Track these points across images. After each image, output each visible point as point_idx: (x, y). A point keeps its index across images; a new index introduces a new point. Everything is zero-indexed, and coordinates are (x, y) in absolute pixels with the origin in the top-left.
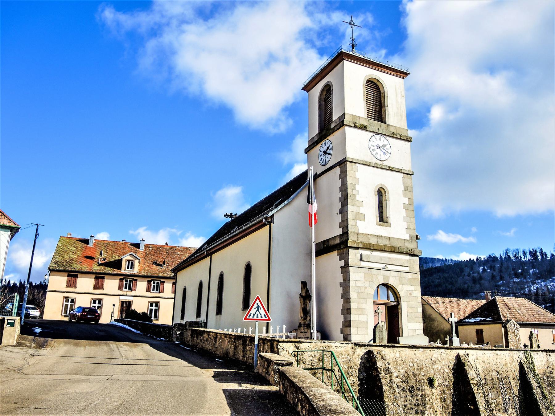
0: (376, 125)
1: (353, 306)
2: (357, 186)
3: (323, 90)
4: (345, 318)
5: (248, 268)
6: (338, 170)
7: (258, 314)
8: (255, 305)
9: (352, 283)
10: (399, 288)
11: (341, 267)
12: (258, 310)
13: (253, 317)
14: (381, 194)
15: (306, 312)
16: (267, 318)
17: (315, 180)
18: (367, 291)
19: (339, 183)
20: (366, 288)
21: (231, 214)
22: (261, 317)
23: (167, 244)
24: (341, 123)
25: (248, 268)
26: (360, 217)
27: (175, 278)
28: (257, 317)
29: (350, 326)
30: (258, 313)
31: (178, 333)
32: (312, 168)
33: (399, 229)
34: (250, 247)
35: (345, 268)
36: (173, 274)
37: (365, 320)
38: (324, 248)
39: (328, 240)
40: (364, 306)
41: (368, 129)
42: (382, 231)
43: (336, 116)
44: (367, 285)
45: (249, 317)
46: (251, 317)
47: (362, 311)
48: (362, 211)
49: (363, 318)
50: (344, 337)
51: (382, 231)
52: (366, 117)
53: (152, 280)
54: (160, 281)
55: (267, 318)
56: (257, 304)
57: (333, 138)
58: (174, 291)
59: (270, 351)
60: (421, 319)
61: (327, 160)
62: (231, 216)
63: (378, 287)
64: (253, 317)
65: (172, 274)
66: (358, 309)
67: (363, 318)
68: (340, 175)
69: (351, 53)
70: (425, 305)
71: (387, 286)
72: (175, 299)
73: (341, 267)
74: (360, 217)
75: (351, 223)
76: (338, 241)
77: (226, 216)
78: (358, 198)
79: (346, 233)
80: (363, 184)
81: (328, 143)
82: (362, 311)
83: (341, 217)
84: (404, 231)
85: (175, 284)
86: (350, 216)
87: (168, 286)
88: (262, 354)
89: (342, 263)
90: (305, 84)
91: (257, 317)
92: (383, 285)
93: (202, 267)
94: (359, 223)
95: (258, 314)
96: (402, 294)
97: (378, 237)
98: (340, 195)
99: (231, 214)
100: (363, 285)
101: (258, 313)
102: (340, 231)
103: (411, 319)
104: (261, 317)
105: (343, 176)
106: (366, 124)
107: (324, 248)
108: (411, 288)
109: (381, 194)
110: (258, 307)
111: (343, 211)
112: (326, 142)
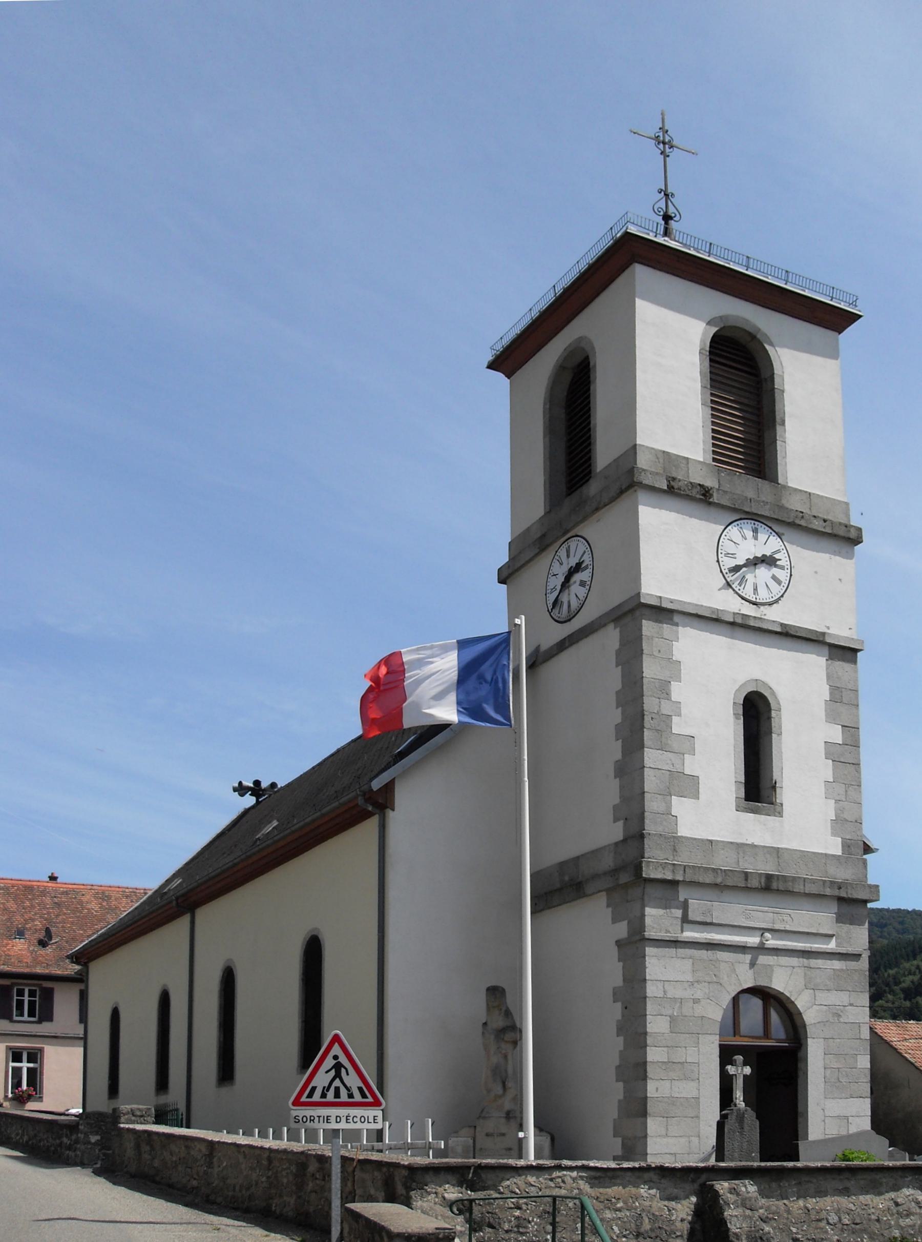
0: (747, 488)
1: (654, 1054)
2: (674, 686)
3: (561, 368)
4: (626, 1091)
5: (313, 952)
6: (611, 637)
7: (337, 1090)
8: (329, 1062)
9: (652, 990)
10: (802, 1002)
11: (619, 943)
12: (338, 1075)
13: (324, 1095)
14: (756, 712)
15: (506, 1078)
16: (370, 1099)
17: (531, 666)
18: (699, 1010)
19: (614, 679)
20: (696, 1001)
21: (257, 783)
22: (351, 1096)
23: (53, 878)
24: (627, 482)
25: (313, 952)
26: (689, 786)
27: (80, 979)
28: (337, 1094)
29: (644, 1114)
30: (337, 1083)
31: (94, 1139)
32: (521, 621)
33: (803, 825)
34: (321, 887)
35: (634, 946)
36: (77, 967)
37: (695, 1094)
38: (559, 888)
39: (576, 860)
40: (691, 1055)
41: (715, 498)
42: (755, 829)
43: (604, 455)
44: (699, 994)
45: (310, 1095)
46: (317, 1097)
47: (682, 1070)
48: (691, 766)
49: (685, 1090)
50: (623, 1144)
51: (755, 829)
52: (710, 461)
53: (13, 985)
54: (40, 986)
55: (370, 1099)
56: (336, 1057)
57: (599, 530)
58: (83, 1018)
59: (381, 1195)
60: (865, 1087)
61: (575, 604)
62: (256, 789)
63: (735, 1000)
64: (324, 1095)
65: (73, 969)
66: (668, 1064)
67: (685, 1090)
68: (618, 653)
69: (661, 240)
70: (878, 1043)
71: (767, 997)
72: (85, 1039)
73: (619, 943)
74: (689, 786)
75: (652, 804)
76: (608, 862)
77: (241, 789)
78: (678, 727)
79: (636, 837)
80: (700, 684)
81: (578, 549)
82: (682, 1070)
83: (622, 788)
84: (826, 829)
85: (83, 997)
86: (651, 782)
87: (65, 1005)
88: (357, 1207)
89: (622, 930)
90: (499, 347)
91: (337, 1094)
92: (754, 991)
93: (167, 944)
94: (680, 806)
95: (337, 1090)
96: (810, 1016)
97: (740, 847)
98: (616, 716)
99: (257, 783)
100: (687, 994)
101: (337, 1083)
102: (616, 832)
103: (835, 1087)
104: (351, 1096)
105: (631, 655)
106: (708, 483)
107: (559, 888)
108: (838, 998)
109: (756, 712)
110: (338, 1067)
111: (630, 769)
112: (573, 543)
